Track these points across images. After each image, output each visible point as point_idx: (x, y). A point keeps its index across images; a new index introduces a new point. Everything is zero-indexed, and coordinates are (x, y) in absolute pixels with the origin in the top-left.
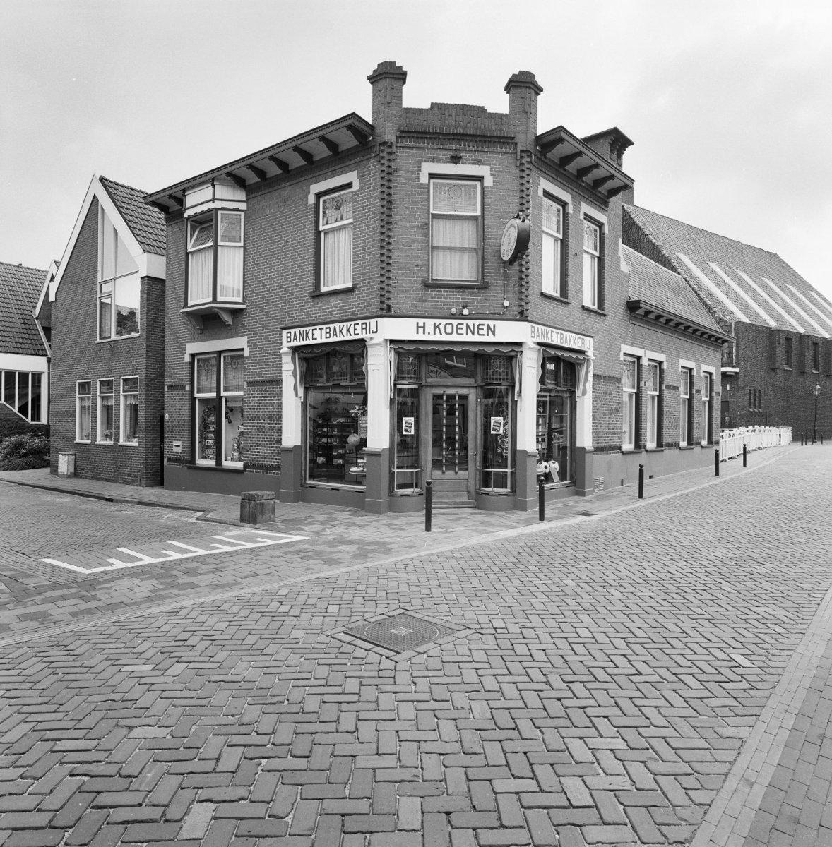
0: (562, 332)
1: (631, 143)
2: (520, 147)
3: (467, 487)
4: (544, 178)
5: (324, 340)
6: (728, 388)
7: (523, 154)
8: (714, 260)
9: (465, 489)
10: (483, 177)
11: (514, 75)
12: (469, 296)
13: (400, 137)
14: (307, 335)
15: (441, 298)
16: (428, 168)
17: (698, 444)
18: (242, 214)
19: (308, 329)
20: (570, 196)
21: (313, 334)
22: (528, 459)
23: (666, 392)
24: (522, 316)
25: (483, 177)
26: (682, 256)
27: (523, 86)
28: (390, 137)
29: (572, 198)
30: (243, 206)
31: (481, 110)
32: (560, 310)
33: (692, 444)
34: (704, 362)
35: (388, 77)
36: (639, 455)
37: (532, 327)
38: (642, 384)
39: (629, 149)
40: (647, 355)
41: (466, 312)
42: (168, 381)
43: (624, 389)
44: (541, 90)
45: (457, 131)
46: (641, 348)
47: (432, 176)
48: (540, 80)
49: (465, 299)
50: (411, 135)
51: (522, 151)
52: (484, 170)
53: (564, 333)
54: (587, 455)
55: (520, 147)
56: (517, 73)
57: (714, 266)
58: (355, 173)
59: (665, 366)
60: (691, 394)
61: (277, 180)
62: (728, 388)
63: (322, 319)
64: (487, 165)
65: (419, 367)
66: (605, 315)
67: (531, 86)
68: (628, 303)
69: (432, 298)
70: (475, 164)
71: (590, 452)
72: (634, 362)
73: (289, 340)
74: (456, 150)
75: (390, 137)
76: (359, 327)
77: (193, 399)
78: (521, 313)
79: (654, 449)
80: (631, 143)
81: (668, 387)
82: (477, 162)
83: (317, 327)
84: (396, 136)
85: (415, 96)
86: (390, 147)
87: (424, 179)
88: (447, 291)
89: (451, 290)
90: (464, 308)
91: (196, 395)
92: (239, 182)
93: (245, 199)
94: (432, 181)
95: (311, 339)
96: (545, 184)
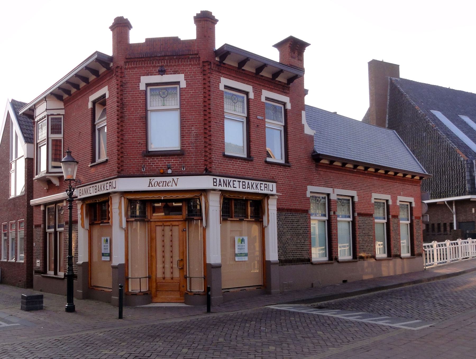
0: (95, 185)
1: (307, 45)
2: (202, 60)
3: (179, 288)
4: (223, 77)
5: (241, 189)
6: (473, 212)
7: (205, 64)
8: (465, 114)
9: (178, 289)
10: (179, 82)
11: (211, 13)
12: (172, 161)
13: (127, 62)
14: (229, 183)
15: (154, 163)
16: (145, 80)
17: (399, 256)
18: (62, 117)
19: (230, 179)
20: (251, 87)
21: (234, 184)
22: (213, 269)
23: (358, 218)
24: (206, 172)
25: (179, 82)
26: (439, 115)
27: (205, 21)
28: (121, 63)
29: (253, 88)
30: (62, 112)
31: (176, 40)
32: (247, 165)
33: (391, 257)
34: (400, 195)
35: (121, 27)
36: (355, 263)
37: (214, 179)
38: (332, 213)
39: (307, 48)
40: (335, 193)
41: (170, 171)
42: (35, 223)
43: (338, 219)
44: (217, 21)
45: (164, 54)
46: (330, 187)
47: (148, 85)
48: (216, 14)
49: (169, 163)
50: (132, 60)
51: (203, 62)
52: (180, 78)
53: (97, 185)
54: (271, 266)
55: (202, 60)
56: (125, 18)
57: (466, 119)
58: (106, 87)
59: (356, 199)
60: (388, 219)
61: (76, 95)
62: (473, 212)
63: (246, 175)
64: (182, 73)
65: (145, 209)
66: (289, 166)
67: (208, 19)
68: (313, 156)
69: (149, 163)
70: (174, 74)
71: (275, 264)
72: (325, 198)
73: (244, 187)
74: (162, 66)
75: (121, 63)
76: (108, 185)
77: (45, 233)
78: (206, 170)
79: (327, 262)
80: (307, 45)
81: (359, 214)
82: (175, 72)
83: (237, 180)
84: (125, 62)
85: (136, 37)
86: (121, 69)
87: (142, 87)
88: (158, 159)
89: (176, 157)
90: (169, 168)
91: (47, 230)
92: (59, 97)
93: (63, 108)
94: (149, 88)
95: (232, 186)
96: (225, 81)
